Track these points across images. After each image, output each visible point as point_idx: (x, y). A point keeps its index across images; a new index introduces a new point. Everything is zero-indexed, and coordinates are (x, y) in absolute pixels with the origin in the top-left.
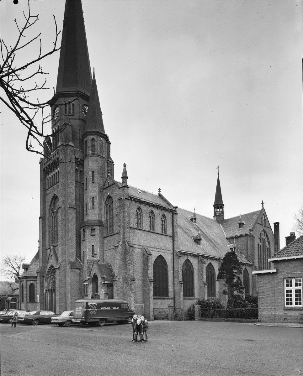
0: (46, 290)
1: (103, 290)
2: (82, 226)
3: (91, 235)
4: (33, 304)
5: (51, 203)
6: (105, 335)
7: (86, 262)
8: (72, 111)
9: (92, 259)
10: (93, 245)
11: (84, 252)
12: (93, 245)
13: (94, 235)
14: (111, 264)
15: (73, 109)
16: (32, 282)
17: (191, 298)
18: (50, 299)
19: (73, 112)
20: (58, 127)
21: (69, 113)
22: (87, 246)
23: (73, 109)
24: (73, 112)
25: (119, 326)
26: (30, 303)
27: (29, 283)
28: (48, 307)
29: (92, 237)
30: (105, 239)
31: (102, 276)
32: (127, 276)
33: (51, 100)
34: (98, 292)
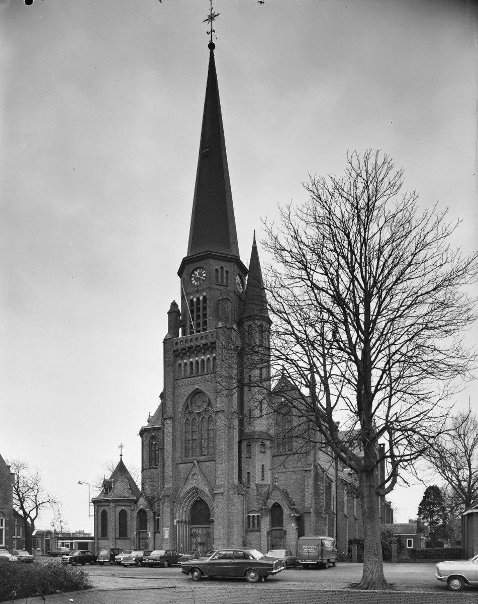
0: (178, 522)
1: (293, 525)
2: (246, 440)
3: (261, 452)
4: (126, 541)
5: (190, 396)
6: (252, 587)
7: (253, 486)
8: (225, 281)
9: (261, 482)
10: (263, 465)
11: (249, 473)
12: (263, 465)
13: (264, 452)
14: (288, 491)
15: (227, 278)
16: (123, 508)
17: (124, 538)
18: (183, 535)
19: (227, 282)
20: (205, 297)
21: (222, 282)
22: (255, 467)
23: (227, 278)
24: (227, 282)
25: (303, 571)
26: (120, 539)
27: (119, 509)
28: (180, 546)
29: (262, 455)
30: (275, 458)
31: (292, 507)
32: (318, 507)
33: (239, 259)
34: (282, 526)
